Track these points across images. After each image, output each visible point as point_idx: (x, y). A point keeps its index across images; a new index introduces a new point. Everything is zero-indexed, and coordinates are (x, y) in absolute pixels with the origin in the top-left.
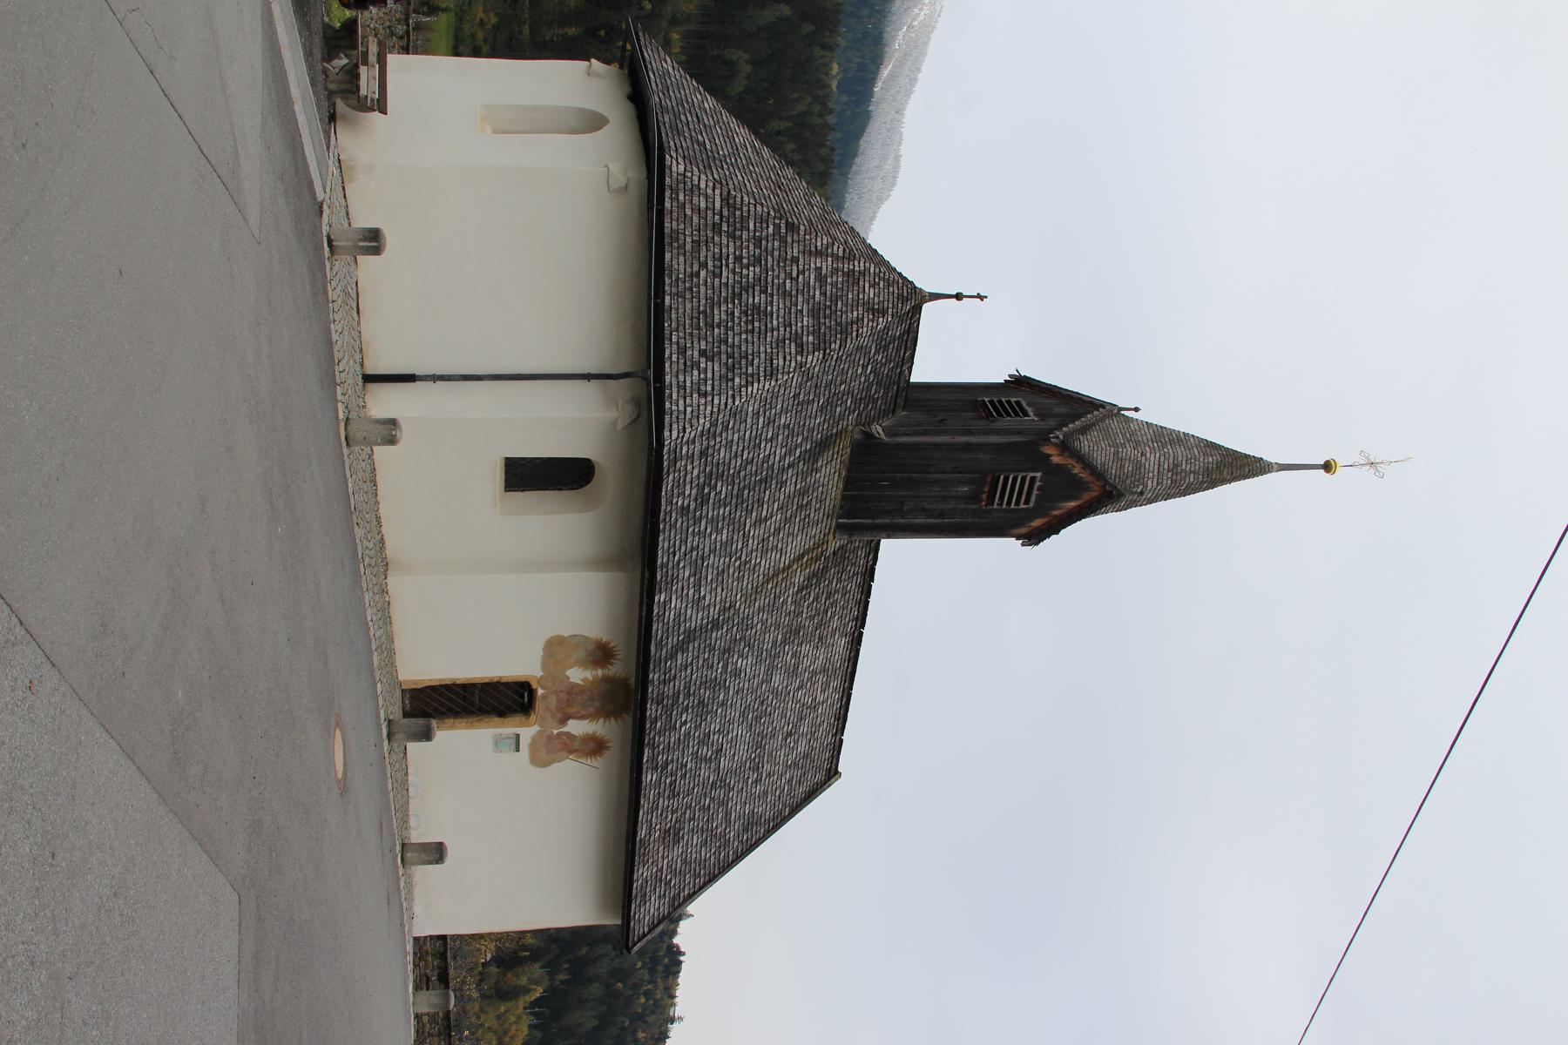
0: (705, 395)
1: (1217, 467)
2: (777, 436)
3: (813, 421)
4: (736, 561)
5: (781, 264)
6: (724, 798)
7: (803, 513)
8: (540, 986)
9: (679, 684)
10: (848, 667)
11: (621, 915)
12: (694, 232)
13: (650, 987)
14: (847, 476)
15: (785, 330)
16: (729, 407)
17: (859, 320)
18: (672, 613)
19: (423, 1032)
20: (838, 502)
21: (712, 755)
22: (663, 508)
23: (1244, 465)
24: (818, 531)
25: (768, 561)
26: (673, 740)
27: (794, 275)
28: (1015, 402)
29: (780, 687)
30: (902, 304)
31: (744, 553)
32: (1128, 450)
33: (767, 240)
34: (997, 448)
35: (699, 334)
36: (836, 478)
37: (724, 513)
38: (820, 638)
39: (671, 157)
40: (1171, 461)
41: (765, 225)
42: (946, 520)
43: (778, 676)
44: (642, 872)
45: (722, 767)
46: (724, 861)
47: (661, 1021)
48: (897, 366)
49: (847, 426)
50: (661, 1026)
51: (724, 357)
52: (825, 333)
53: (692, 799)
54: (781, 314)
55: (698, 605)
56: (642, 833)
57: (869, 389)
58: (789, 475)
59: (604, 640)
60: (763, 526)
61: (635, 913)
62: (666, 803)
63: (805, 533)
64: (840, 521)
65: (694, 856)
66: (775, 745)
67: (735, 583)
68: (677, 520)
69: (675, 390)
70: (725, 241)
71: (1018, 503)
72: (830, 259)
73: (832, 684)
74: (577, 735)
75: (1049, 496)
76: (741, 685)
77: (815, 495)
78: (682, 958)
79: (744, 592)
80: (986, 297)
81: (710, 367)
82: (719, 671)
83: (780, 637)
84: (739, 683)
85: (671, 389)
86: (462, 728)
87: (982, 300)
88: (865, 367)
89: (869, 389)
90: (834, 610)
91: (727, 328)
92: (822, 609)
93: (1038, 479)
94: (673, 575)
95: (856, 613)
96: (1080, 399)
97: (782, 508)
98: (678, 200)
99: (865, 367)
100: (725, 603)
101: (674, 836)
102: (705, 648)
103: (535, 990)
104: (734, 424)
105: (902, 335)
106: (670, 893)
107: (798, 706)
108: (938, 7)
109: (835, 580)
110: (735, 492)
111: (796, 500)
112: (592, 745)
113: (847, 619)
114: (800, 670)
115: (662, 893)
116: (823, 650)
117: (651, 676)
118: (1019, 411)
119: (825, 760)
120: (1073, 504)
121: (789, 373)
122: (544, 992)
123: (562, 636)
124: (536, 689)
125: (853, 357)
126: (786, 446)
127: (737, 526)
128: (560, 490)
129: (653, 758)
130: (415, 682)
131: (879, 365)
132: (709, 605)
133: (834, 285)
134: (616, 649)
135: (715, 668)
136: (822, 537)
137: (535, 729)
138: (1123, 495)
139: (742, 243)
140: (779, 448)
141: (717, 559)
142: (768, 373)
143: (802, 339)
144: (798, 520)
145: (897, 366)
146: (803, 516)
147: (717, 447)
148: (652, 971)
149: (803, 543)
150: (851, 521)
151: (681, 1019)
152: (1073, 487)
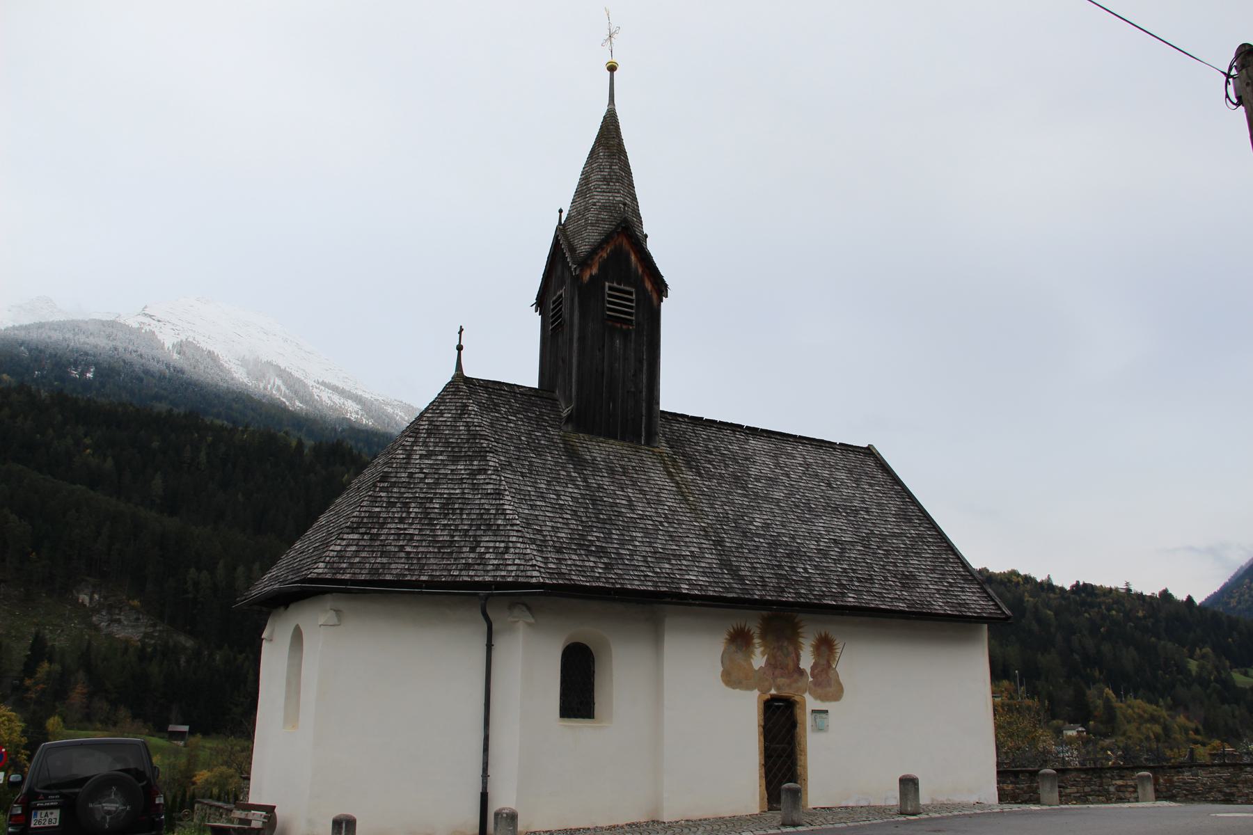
0: (507, 548)
1: (608, 149)
2: (556, 490)
3: (549, 462)
4: (663, 526)
5: (412, 486)
6: (879, 538)
7: (630, 471)
8: (1103, 689)
9: (768, 573)
10: (775, 438)
11: (979, 625)
12: (374, 555)
13: (1103, 607)
14: (604, 436)
15: (465, 483)
16: (520, 529)
17: (467, 425)
18: (701, 578)
19: (1099, 791)
20: (626, 444)
21: (838, 548)
22: (601, 584)
23: (608, 129)
24: (649, 460)
25: (668, 499)
26: (819, 580)
27: (422, 476)
28: (553, 305)
29: (785, 492)
30: (461, 392)
31: (656, 519)
32: (591, 216)
33: (391, 497)
34: (583, 316)
35: (456, 552)
36: (604, 445)
37: (617, 535)
38: (746, 459)
39: (311, 573)
40: (601, 183)
41: (379, 499)
42: (645, 357)
43: (775, 493)
44: (939, 606)
45: (851, 540)
46: (936, 539)
47: (1130, 599)
48: (515, 396)
49: (559, 435)
50: (1133, 599)
51: (479, 533)
52: (473, 452)
53: (877, 564)
54: (452, 486)
55: (698, 557)
56: (902, 606)
57: (530, 418)
58: (593, 481)
59: (727, 637)
60: (635, 503)
61: (975, 613)
62: (877, 586)
63: (649, 470)
64: (643, 442)
65: (929, 563)
66: (836, 496)
67: (684, 526)
68: (616, 573)
69: (498, 573)
70: (385, 531)
71: (631, 301)
72: (415, 448)
73: (789, 451)
74: (813, 661)
75: (625, 274)
76: (778, 523)
77: (615, 462)
78: (1081, 583)
79: (692, 519)
80: (461, 327)
81: (485, 544)
82: (762, 540)
83: (739, 491)
84: (776, 525)
85: (497, 576)
86: (806, 759)
87: (463, 330)
88: (510, 421)
89: (530, 418)
90: (722, 448)
91: (456, 530)
92: (720, 458)
93: (611, 284)
94: (666, 577)
95: (728, 431)
96: (552, 255)
97: (622, 488)
98: (346, 568)
99: (510, 421)
100: (700, 535)
101: (909, 579)
102: (738, 552)
103: (1106, 694)
104: (537, 525)
105: (487, 392)
106: (960, 583)
107: (804, 478)
108: (396, 403)
109: (696, 447)
110: (599, 525)
111: (617, 477)
112: (823, 648)
113: (732, 438)
114: (772, 476)
115: (959, 589)
116: (758, 458)
117: (757, 597)
118: (558, 302)
119: (855, 457)
120: (633, 258)
121: (501, 480)
122: (1108, 687)
124: (771, 695)
125: (498, 430)
126: (566, 484)
127: (631, 525)
128: (594, 672)
129: (834, 596)
130: (762, 799)
131: (511, 410)
132: (700, 548)
133: (436, 445)
134: (735, 627)
135: (759, 544)
136: (655, 457)
137: (807, 696)
138: (625, 218)
139: (389, 517)
140: (567, 489)
141: (659, 541)
142: (498, 497)
143: (475, 470)
144: (635, 476)
145: (515, 396)
146: (633, 472)
147: (556, 539)
148: (1091, 606)
149: (658, 472)
150: (643, 434)
151: (1127, 584)
152: (618, 257)
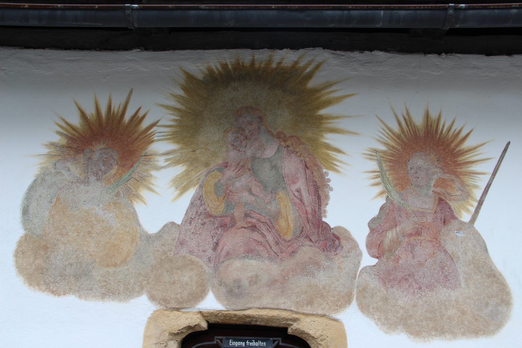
59: (57, 139)
74: (382, 201)
123: (20, 244)
134: (90, 111)
